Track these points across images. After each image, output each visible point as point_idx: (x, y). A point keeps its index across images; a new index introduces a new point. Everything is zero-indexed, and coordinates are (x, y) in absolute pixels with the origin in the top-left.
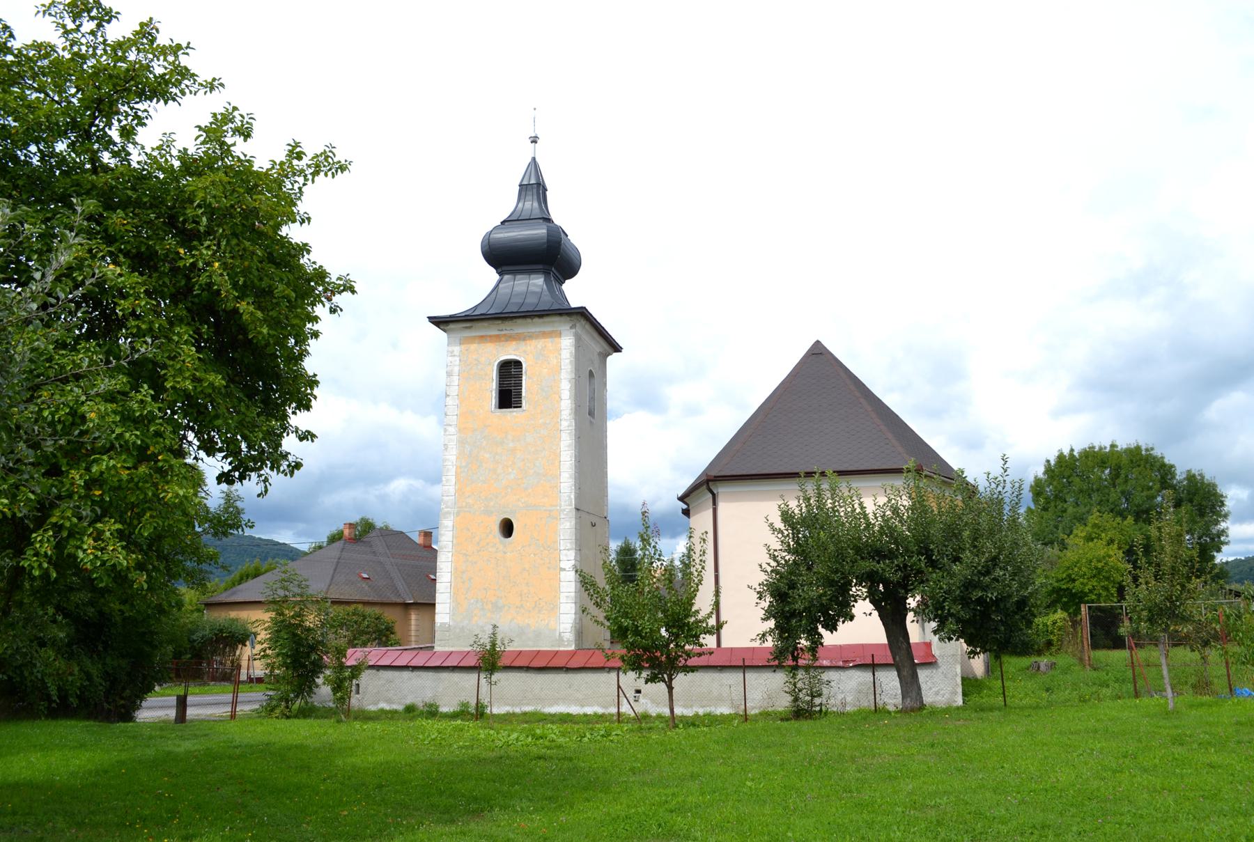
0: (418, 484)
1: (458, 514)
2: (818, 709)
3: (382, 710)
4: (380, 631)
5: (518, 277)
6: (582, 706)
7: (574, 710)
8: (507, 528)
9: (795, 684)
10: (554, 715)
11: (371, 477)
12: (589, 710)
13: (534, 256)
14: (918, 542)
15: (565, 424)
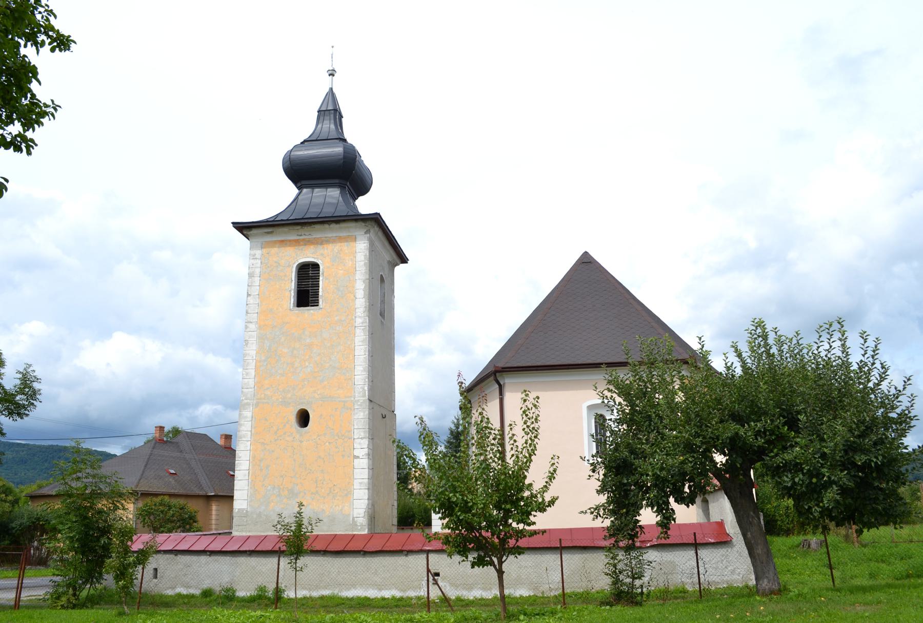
0: (219, 407)
1: (257, 405)
2: (640, 590)
3: (180, 595)
4: (183, 520)
5: (316, 190)
6: (380, 590)
7: (372, 593)
8: (304, 418)
9: (615, 566)
10: (352, 599)
11: (181, 404)
12: (387, 594)
13: (329, 173)
14: (778, 405)
15: (359, 321)
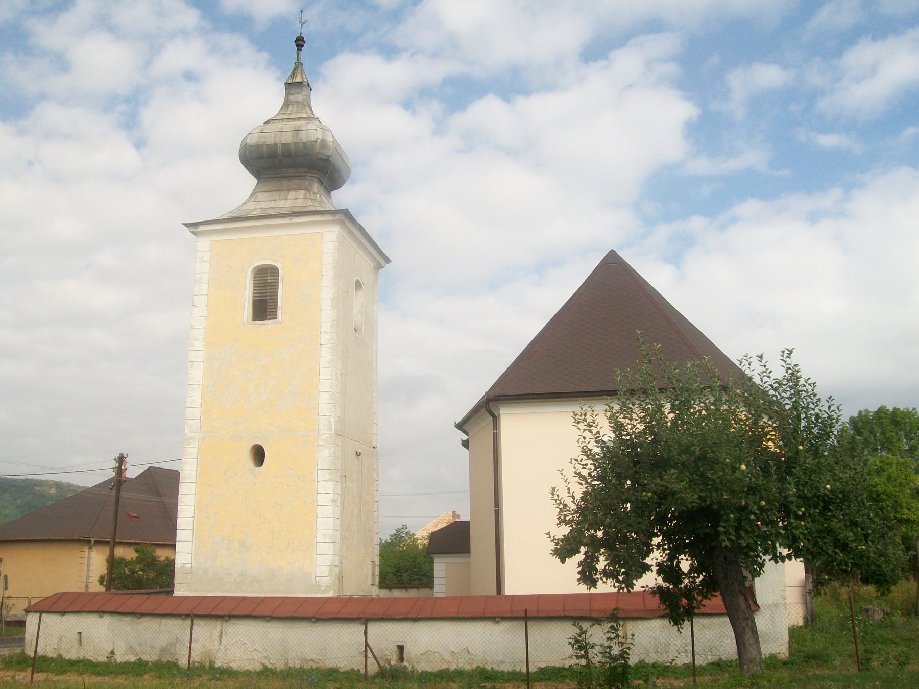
8: (259, 455)
15: (325, 338)
